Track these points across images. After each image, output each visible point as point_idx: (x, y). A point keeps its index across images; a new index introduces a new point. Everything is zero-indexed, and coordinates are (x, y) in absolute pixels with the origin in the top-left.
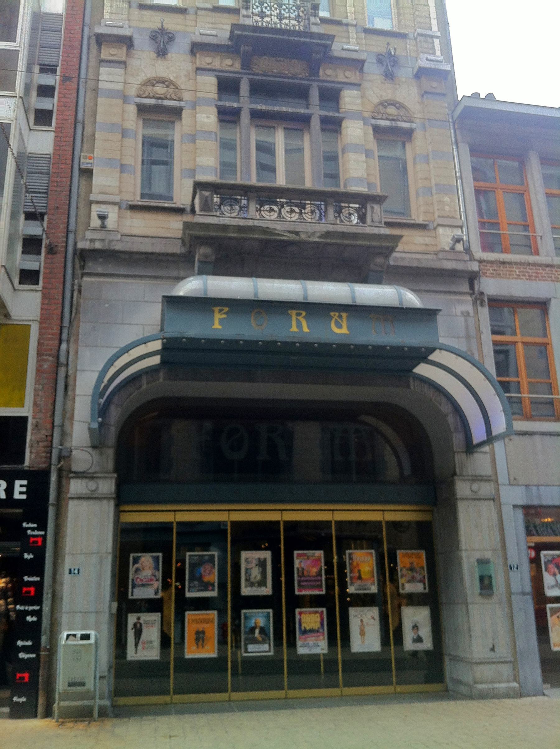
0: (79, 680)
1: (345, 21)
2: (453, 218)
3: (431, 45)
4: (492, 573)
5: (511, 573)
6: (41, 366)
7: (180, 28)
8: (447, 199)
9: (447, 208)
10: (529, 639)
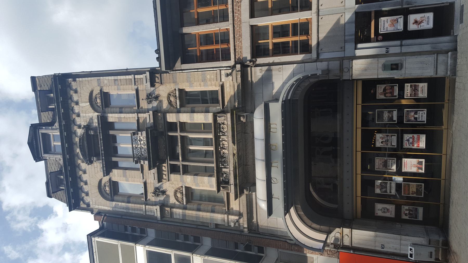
0: (429, 254)
1: (137, 119)
2: (216, 74)
3: (139, 80)
4: (390, 63)
5: (390, 52)
6: (296, 250)
7: (152, 185)
8: (208, 77)
9: (212, 77)
10: (426, 44)
